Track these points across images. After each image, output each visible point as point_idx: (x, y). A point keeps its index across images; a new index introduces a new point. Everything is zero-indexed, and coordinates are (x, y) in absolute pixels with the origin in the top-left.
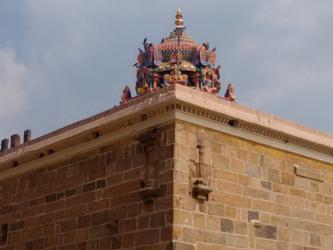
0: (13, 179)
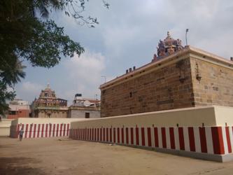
0: (132, 80)
